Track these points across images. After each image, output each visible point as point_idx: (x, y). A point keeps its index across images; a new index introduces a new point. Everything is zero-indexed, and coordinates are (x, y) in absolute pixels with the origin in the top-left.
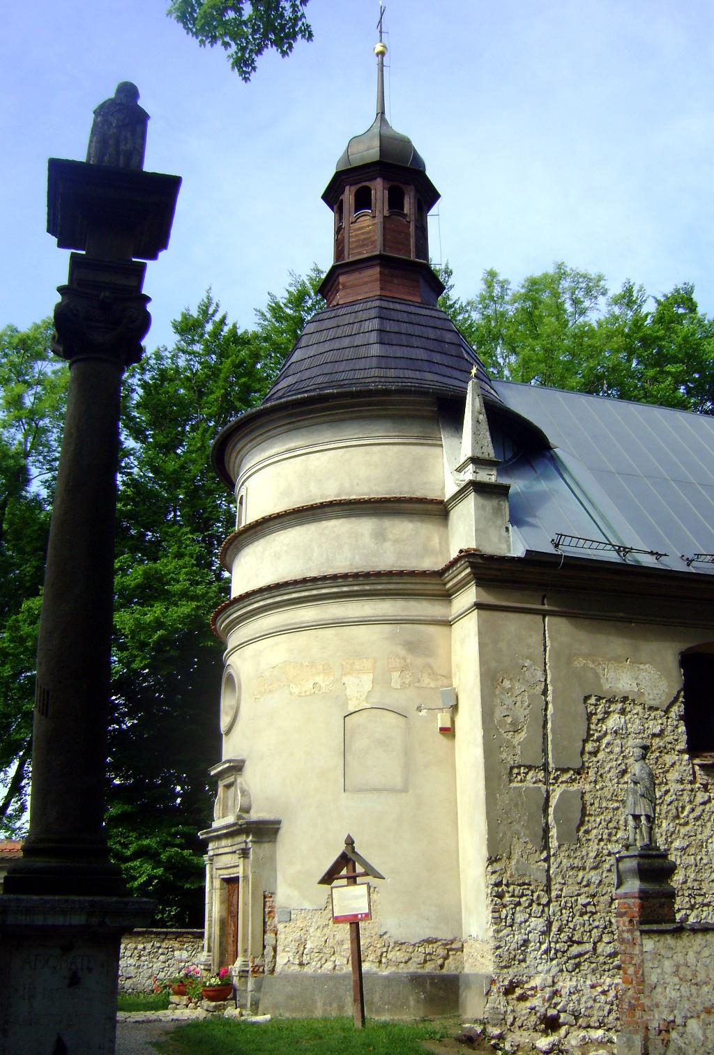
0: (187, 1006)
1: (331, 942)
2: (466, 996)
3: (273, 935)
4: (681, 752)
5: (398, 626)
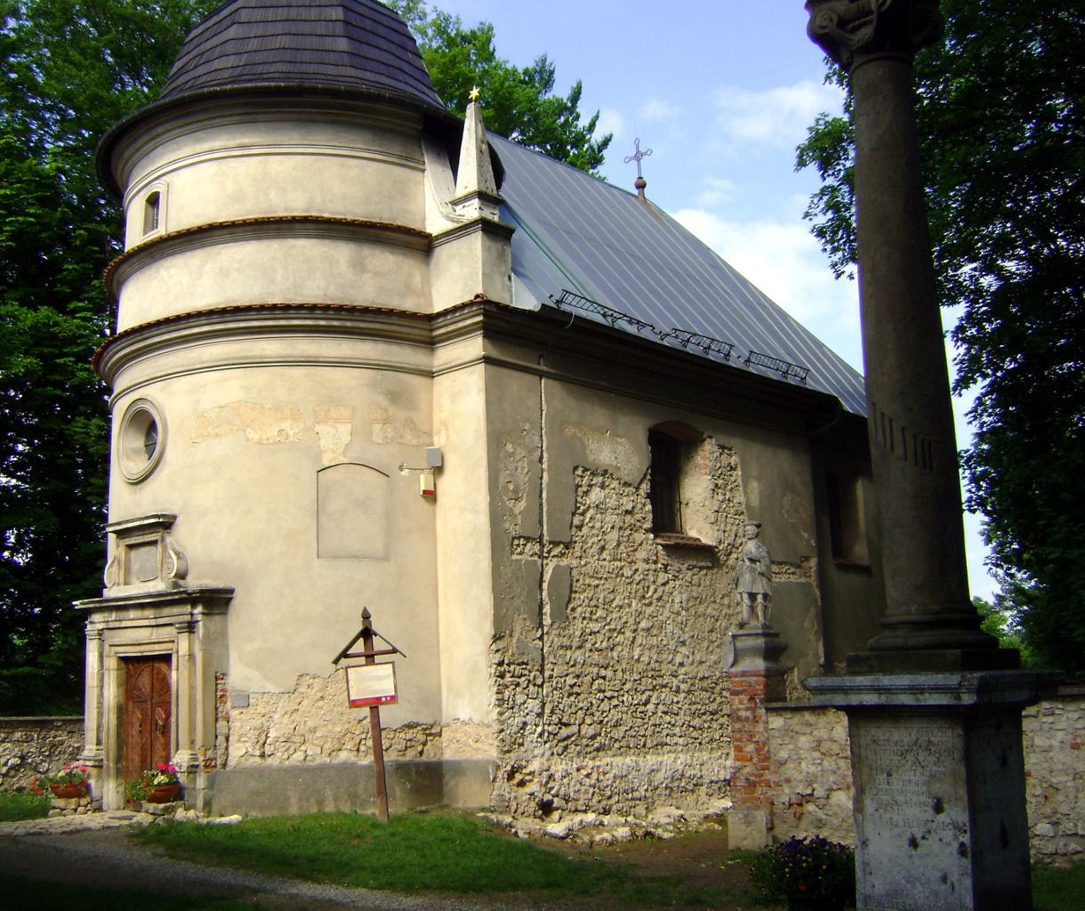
0: (76, 810)
1: (301, 729)
2: (456, 785)
3: (225, 723)
4: (647, 531)
5: (380, 372)
